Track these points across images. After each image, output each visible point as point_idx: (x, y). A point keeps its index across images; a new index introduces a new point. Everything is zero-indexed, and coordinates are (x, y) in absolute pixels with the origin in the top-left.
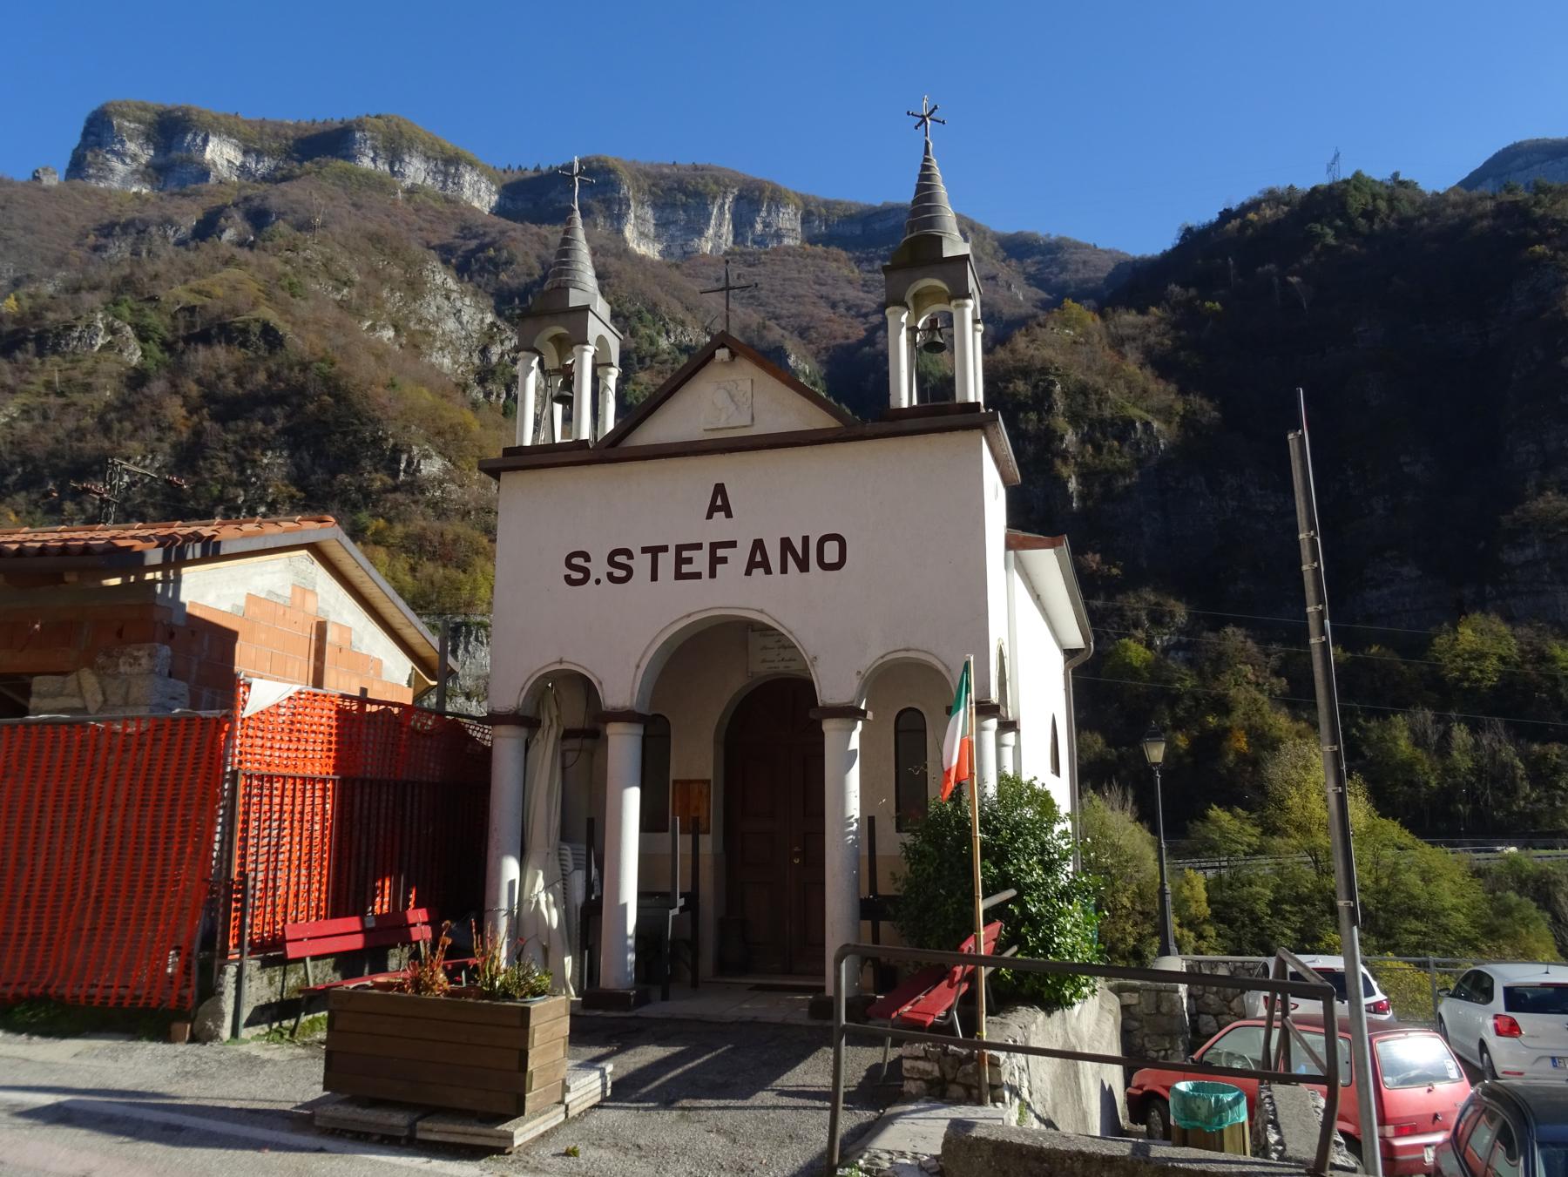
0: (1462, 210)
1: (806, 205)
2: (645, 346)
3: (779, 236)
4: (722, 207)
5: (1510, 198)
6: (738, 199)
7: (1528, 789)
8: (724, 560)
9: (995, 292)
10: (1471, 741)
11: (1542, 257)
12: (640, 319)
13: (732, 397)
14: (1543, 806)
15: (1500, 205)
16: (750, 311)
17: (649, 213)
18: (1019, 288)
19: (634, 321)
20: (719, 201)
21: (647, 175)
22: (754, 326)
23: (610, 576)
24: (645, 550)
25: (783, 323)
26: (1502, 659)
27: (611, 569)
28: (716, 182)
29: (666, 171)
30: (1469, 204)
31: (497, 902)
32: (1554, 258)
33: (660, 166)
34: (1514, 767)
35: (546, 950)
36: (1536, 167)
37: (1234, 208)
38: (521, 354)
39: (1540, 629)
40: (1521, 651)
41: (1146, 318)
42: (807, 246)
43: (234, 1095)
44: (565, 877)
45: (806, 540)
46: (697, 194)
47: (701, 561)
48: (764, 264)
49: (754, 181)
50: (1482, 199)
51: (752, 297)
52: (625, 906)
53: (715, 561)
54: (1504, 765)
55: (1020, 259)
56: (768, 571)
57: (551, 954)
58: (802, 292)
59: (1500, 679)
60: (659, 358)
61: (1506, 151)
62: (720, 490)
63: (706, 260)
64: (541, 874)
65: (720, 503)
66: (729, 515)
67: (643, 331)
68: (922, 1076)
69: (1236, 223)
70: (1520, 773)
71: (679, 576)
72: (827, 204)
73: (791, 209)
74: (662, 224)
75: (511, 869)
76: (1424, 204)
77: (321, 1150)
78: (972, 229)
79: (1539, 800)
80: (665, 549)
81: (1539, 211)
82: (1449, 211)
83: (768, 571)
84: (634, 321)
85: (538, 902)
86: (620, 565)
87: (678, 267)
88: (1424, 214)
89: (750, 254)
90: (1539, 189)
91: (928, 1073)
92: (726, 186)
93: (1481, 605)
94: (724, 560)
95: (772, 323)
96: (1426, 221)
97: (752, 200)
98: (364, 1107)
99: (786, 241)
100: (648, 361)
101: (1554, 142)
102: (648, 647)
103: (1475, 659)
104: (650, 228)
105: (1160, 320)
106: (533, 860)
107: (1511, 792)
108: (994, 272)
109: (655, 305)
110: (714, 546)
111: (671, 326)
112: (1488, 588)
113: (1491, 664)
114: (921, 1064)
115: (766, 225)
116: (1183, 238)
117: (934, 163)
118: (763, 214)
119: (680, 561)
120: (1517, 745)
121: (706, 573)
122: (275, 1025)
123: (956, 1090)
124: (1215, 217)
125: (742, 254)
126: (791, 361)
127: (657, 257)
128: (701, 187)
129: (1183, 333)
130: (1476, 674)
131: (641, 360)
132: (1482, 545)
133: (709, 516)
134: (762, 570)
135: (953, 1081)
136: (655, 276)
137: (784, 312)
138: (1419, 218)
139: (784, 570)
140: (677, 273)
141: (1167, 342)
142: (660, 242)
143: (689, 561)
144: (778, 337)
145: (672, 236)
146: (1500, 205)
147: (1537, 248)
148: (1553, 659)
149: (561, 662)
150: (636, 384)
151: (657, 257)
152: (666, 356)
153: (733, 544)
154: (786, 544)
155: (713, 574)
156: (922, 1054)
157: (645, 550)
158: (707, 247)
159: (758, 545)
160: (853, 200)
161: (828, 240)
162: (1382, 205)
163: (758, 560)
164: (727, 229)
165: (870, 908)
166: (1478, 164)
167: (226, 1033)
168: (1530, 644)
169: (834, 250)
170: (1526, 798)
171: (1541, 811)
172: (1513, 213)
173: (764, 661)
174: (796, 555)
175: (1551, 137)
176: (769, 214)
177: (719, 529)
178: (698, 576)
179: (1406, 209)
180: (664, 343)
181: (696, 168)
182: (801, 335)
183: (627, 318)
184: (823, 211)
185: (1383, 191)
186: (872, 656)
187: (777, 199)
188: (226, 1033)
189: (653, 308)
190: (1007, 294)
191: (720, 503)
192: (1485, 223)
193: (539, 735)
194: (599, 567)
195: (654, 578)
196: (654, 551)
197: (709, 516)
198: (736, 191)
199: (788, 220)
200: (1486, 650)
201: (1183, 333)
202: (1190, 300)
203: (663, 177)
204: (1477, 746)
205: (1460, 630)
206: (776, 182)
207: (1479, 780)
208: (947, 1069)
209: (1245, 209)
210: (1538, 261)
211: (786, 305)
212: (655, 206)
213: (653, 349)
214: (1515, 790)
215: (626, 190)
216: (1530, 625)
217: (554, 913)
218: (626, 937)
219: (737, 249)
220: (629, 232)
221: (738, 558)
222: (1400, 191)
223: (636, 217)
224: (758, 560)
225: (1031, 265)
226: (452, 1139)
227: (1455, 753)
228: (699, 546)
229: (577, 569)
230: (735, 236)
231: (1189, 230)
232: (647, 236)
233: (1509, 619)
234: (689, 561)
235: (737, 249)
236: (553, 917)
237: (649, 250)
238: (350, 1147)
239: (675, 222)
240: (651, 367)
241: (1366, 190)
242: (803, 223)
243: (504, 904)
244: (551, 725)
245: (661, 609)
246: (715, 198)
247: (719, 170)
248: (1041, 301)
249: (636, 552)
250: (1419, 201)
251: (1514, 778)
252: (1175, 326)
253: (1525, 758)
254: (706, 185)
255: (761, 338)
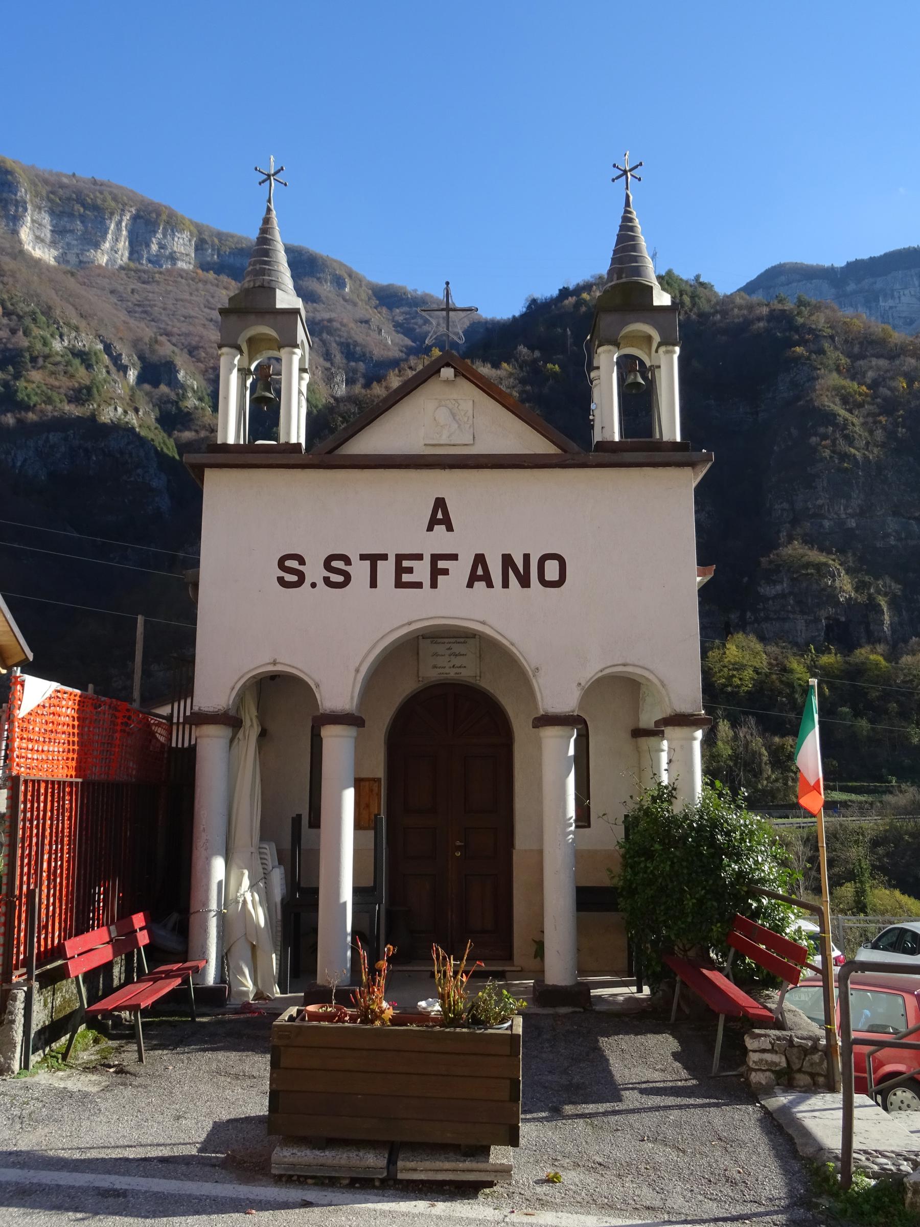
0: (745, 312)
1: (200, 233)
2: (39, 346)
3: (173, 258)
4: (119, 223)
5: (780, 307)
6: (135, 218)
7: (770, 772)
8: (445, 572)
9: (368, 335)
10: (731, 733)
11: (800, 357)
12: (35, 320)
13: (454, 415)
14: (779, 784)
15: (772, 311)
16: (142, 325)
17: (46, 219)
18: (388, 333)
19: (28, 321)
20: (116, 218)
21: (46, 182)
22: (147, 340)
23: (327, 580)
24: (363, 557)
25: (174, 340)
26: (756, 671)
27: (328, 574)
28: (115, 199)
29: (65, 180)
30: (750, 308)
31: (206, 903)
32: (808, 358)
33: (59, 175)
34: (760, 755)
35: (254, 948)
36: (795, 284)
37: (571, 287)
38: (225, 350)
39: (784, 648)
40: (770, 664)
41: (499, 372)
42: (200, 271)
43: (100, 1142)
44: (266, 877)
45: (527, 557)
46: (95, 208)
47: (421, 571)
48: (158, 283)
49: (152, 203)
50: (760, 304)
51: (145, 312)
52: (345, 903)
53: (436, 573)
54: (754, 753)
55: (390, 308)
56: (490, 585)
57: (259, 953)
58: (192, 313)
59: (754, 685)
60: (51, 360)
61: (774, 268)
62: (440, 503)
63: (102, 272)
64: (246, 872)
65: (440, 516)
66: (450, 528)
67: (36, 332)
68: (770, 1067)
69: (572, 300)
70: (765, 759)
71: (399, 584)
72: (219, 235)
73: (186, 235)
74: (59, 232)
75: (218, 866)
76: (717, 303)
77: (306, 1204)
78: (350, 276)
79: (776, 780)
80: (384, 557)
81: (800, 320)
82: (736, 310)
83: (490, 585)
84: (28, 321)
85: (245, 902)
86: (337, 573)
87: (72, 274)
88: (717, 312)
89: (144, 272)
90: (801, 303)
91: (776, 1064)
92: (124, 204)
93: (742, 626)
94: (445, 572)
95: (163, 339)
96: (718, 317)
97: (147, 222)
98: (322, 1148)
99: (180, 264)
100: (40, 361)
101: (807, 266)
102: (369, 652)
103: (736, 669)
104: (47, 234)
105: (511, 375)
106: (237, 858)
107: (757, 774)
108: (368, 317)
109: (50, 308)
110: (435, 558)
111: (65, 330)
112: (749, 614)
113: (748, 673)
114: (768, 1057)
115: (162, 247)
116: (529, 307)
117: (634, 215)
118: (159, 235)
119: (400, 570)
120: (764, 738)
121: (427, 583)
122: (47, 1049)
123: (803, 1079)
124: (555, 293)
125: (136, 271)
126: (181, 375)
127: (52, 262)
128: (99, 202)
129: (528, 388)
130: (737, 681)
131: (34, 360)
132: (746, 579)
133: (430, 528)
134: (484, 583)
135: (800, 1071)
136: (51, 280)
137: (175, 330)
138: (714, 314)
139: (506, 585)
140: (72, 280)
141: (515, 394)
142: (56, 249)
143: (410, 570)
144: (168, 352)
145: (68, 244)
146: (772, 311)
147: (798, 349)
148: (791, 671)
149: (275, 663)
150: (28, 381)
151: (52, 262)
152: (59, 359)
153: (454, 557)
154: (507, 561)
155: (434, 585)
156: (769, 1047)
157: (363, 557)
158: (103, 260)
159: (480, 559)
160: (245, 235)
161: (220, 268)
162: (687, 299)
163: (479, 573)
164: (123, 245)
165: (588, 899)
166: (753, 276)
167: (16, 1065)
168: (776, 659)
169: (224, 278)
170: (768, 779)
171: (778, 789)
172: (781, 319)
173: (435, 667)
174: (518, 572)
175: (806, 262)
176: (165, 236)
177: (440, 541)
178: (419, 585)
179: (706, 307)
180: (57, 346)
181: (95, 182)
182: (190, 353)
183: (20, 318)
184: (216, 241)
185: (688, 289)
186: (591, 671)
187: (173, 224)
188: (16, 1065)
189: (48, 311)
190: (377, 337)
191: (440, 516)
192: (761, 324)
193: (240, 735)
194: (314, 571)
195: (373, 584)
196: (374, 559)
197: (430, 528)
198: (133, 210)
199: (182, 245)
200: (745, 662)
201: (528, 388)
202: (535, 361)
203: (62, 186)
204: (736, 738)
205: (728, 646)
206: (174, 207)
207: (735, 765)
208: (794, 1059)
209: (579, 290)
210: (797, 359)
211: (178, 324)
212: (52, 213)
213: (47, 350)
214: (761, 772)
215: (23, 192)
216: (777, 644)
217: (260, 911)
218: (346, 934)
219: (132, 265)
220: (25, 234)
221: (460, 570)
222: (700, 290)
223: (33, 221)
224: (479, 573)
225: (399, 314)
226: (440, 1177)
227: (720, 743)
228: (419, 557)
229: (291, 570)
230: (131, 253)
231: (534, 301)
232: (42, 241)
233: (762, 639)
234: (410, 570)
235: (132, 265)
236: (260, 916)
237: (45, 254)
238: (348, 1196)
239: (72, 231)
240: (43, 367)
241: (676, 285)
242: (197, 249)
243: (214, 906)
244: (252, 725)
245: (379, 616)
246: (112, 214)
247: (118, 187)
248: (406, 347)
249: (354, 559)
250: (714, 300)
251: (760, 763)
252: (523, 381)
253: (768, 748)
254: (104, 200)
255: (153, 351)
